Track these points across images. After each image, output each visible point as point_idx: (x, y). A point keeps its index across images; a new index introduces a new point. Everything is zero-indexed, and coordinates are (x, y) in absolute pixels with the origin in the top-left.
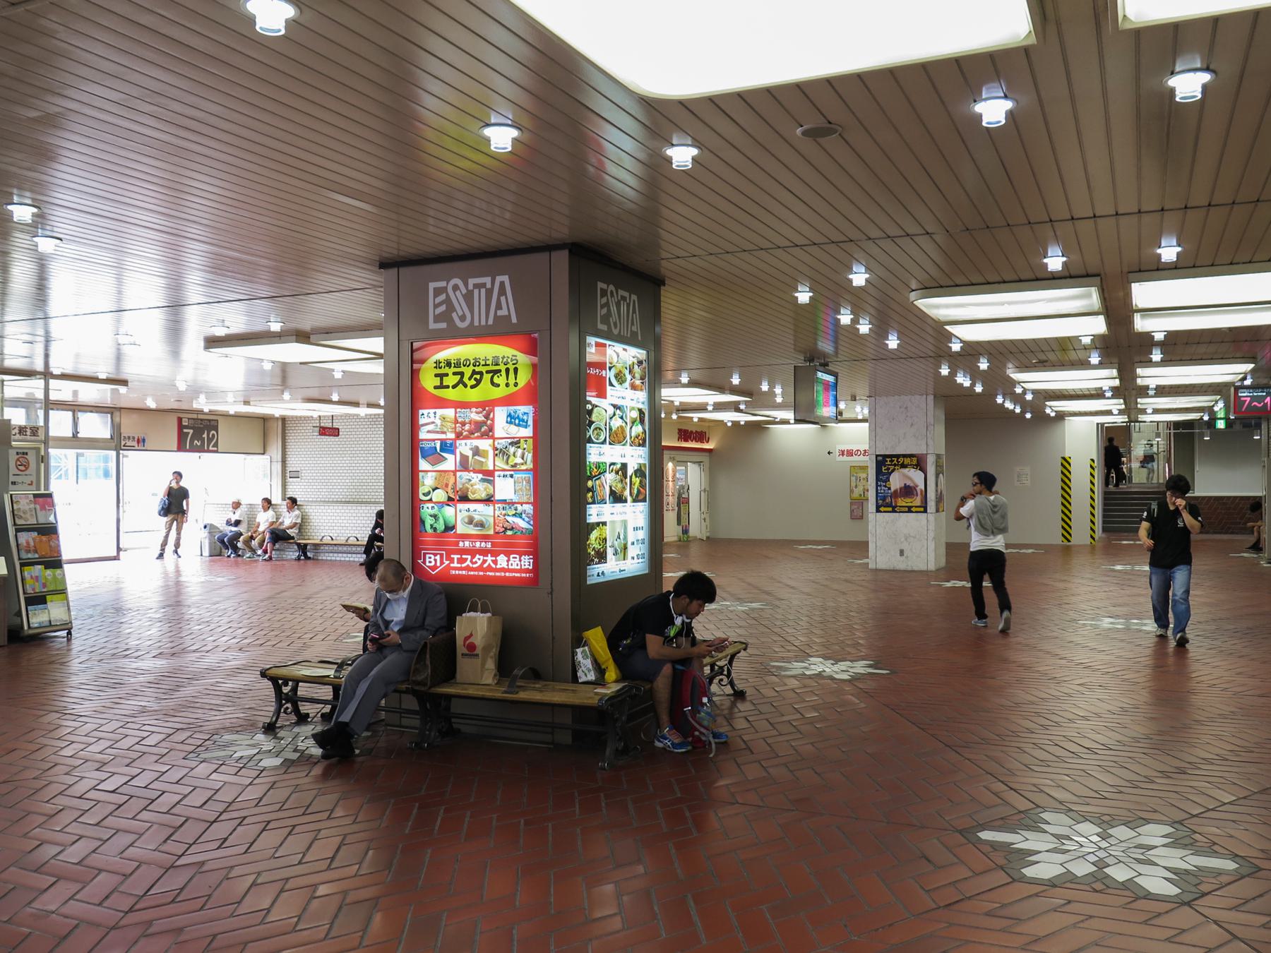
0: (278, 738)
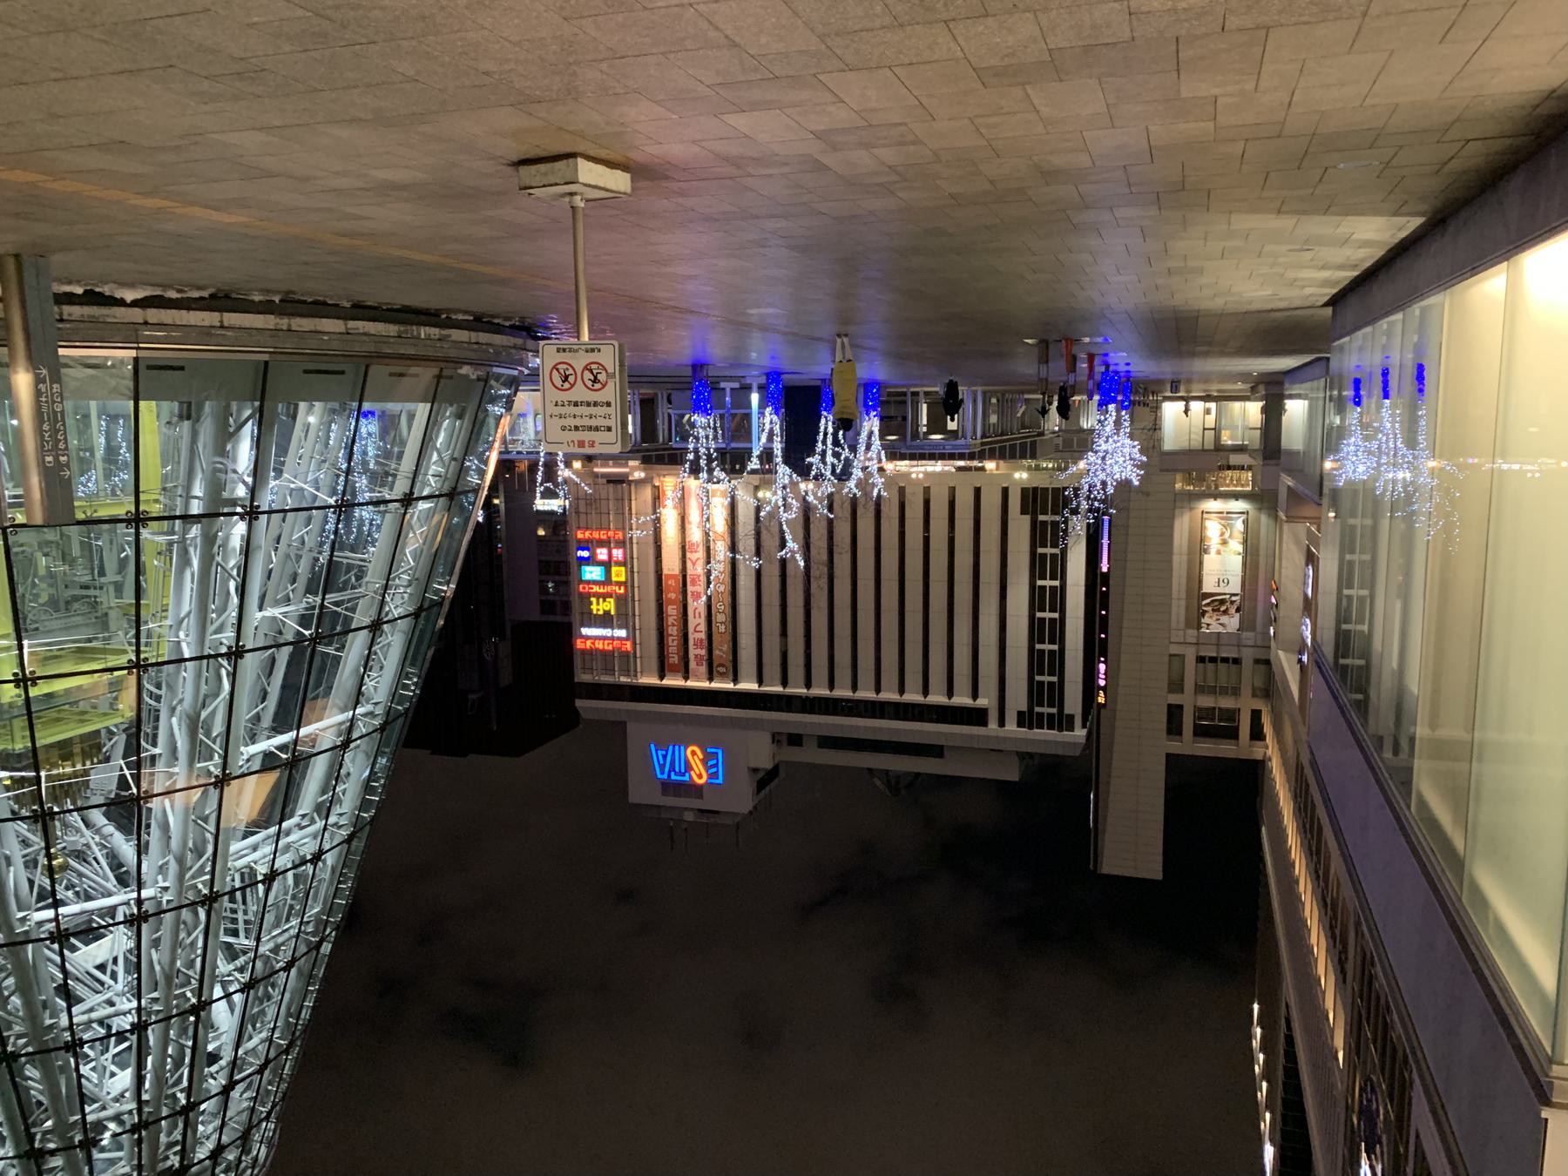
0: (1257, 384)
